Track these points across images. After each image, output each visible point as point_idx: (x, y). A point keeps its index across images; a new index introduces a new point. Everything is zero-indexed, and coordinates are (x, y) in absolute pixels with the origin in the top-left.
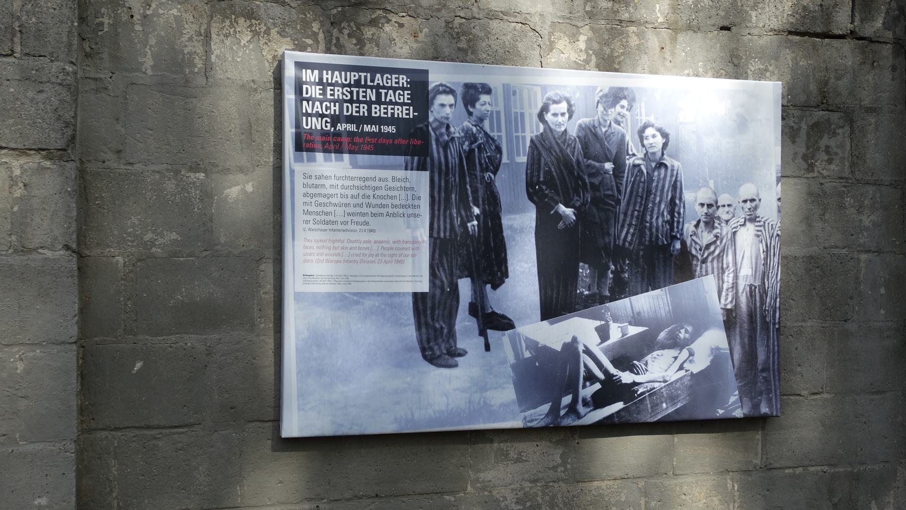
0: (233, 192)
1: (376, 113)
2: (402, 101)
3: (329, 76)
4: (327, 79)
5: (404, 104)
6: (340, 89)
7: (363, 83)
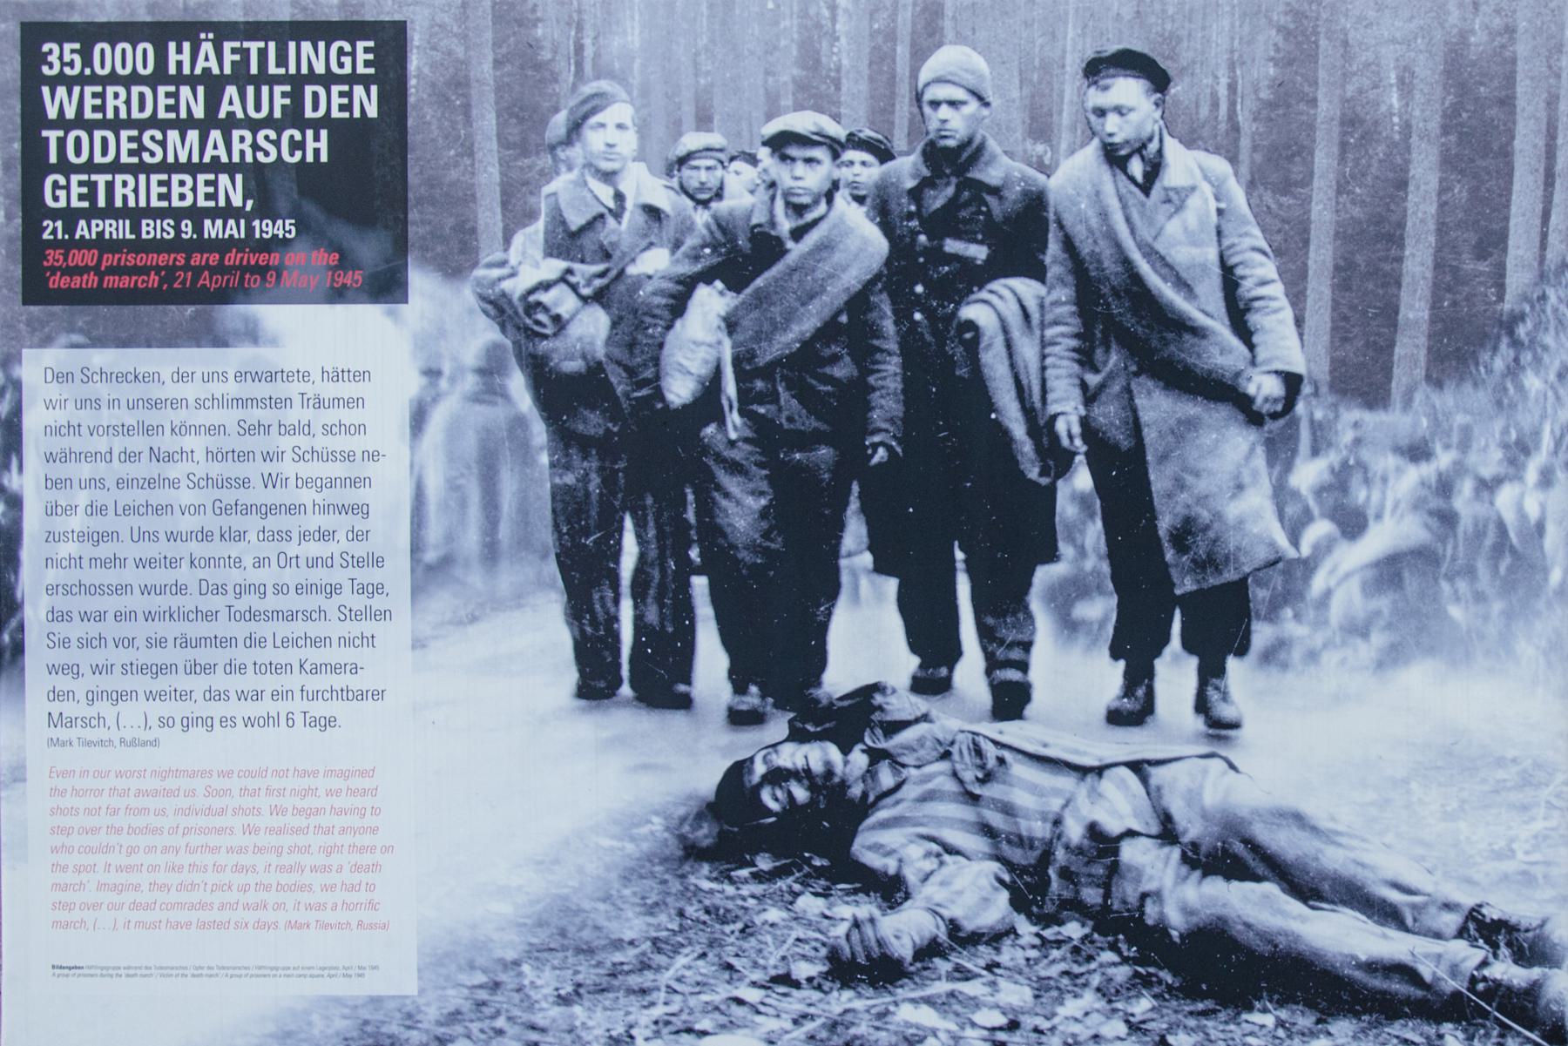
0: (1114, 358)
1: (182, 197)
2: (348, 70)
3: (186, 57)
4: (179, 64)
5: (353, 79)
6: (248, 135)
7: (254, 70)
